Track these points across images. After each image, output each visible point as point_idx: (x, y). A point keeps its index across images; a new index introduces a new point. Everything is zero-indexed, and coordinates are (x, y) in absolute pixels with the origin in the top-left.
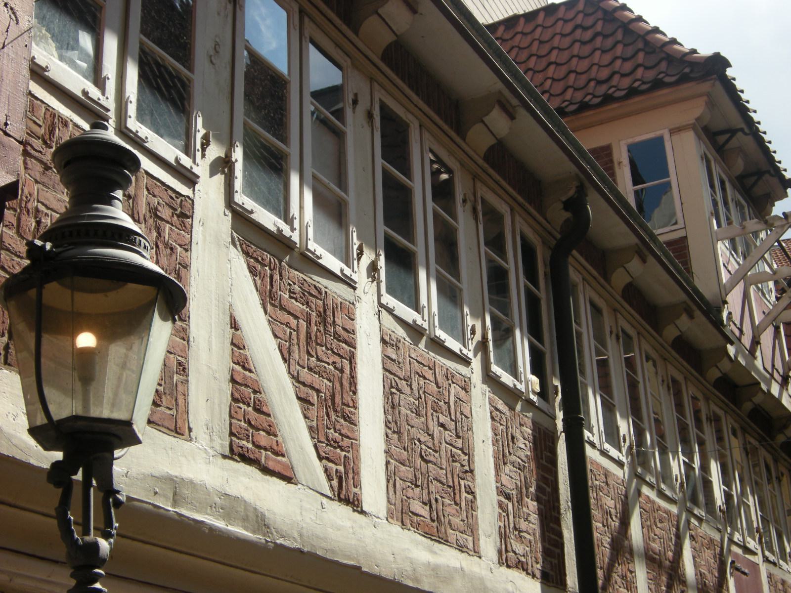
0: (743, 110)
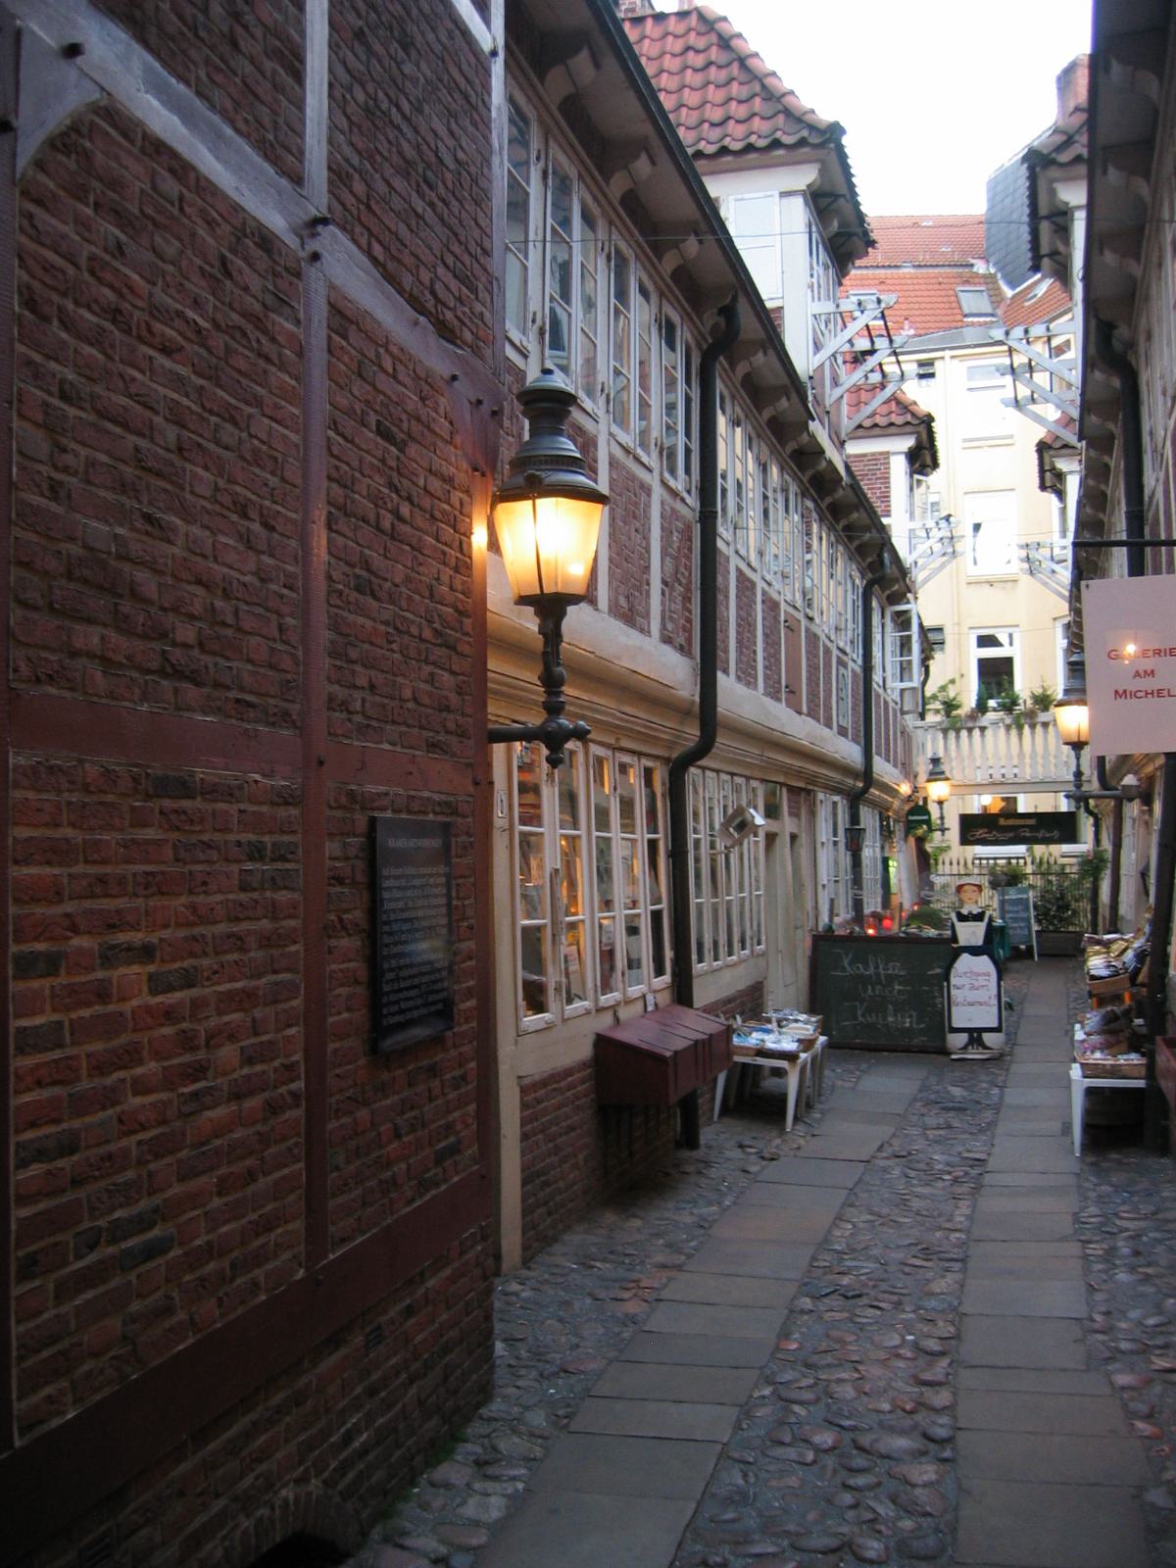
0: (851, 186)
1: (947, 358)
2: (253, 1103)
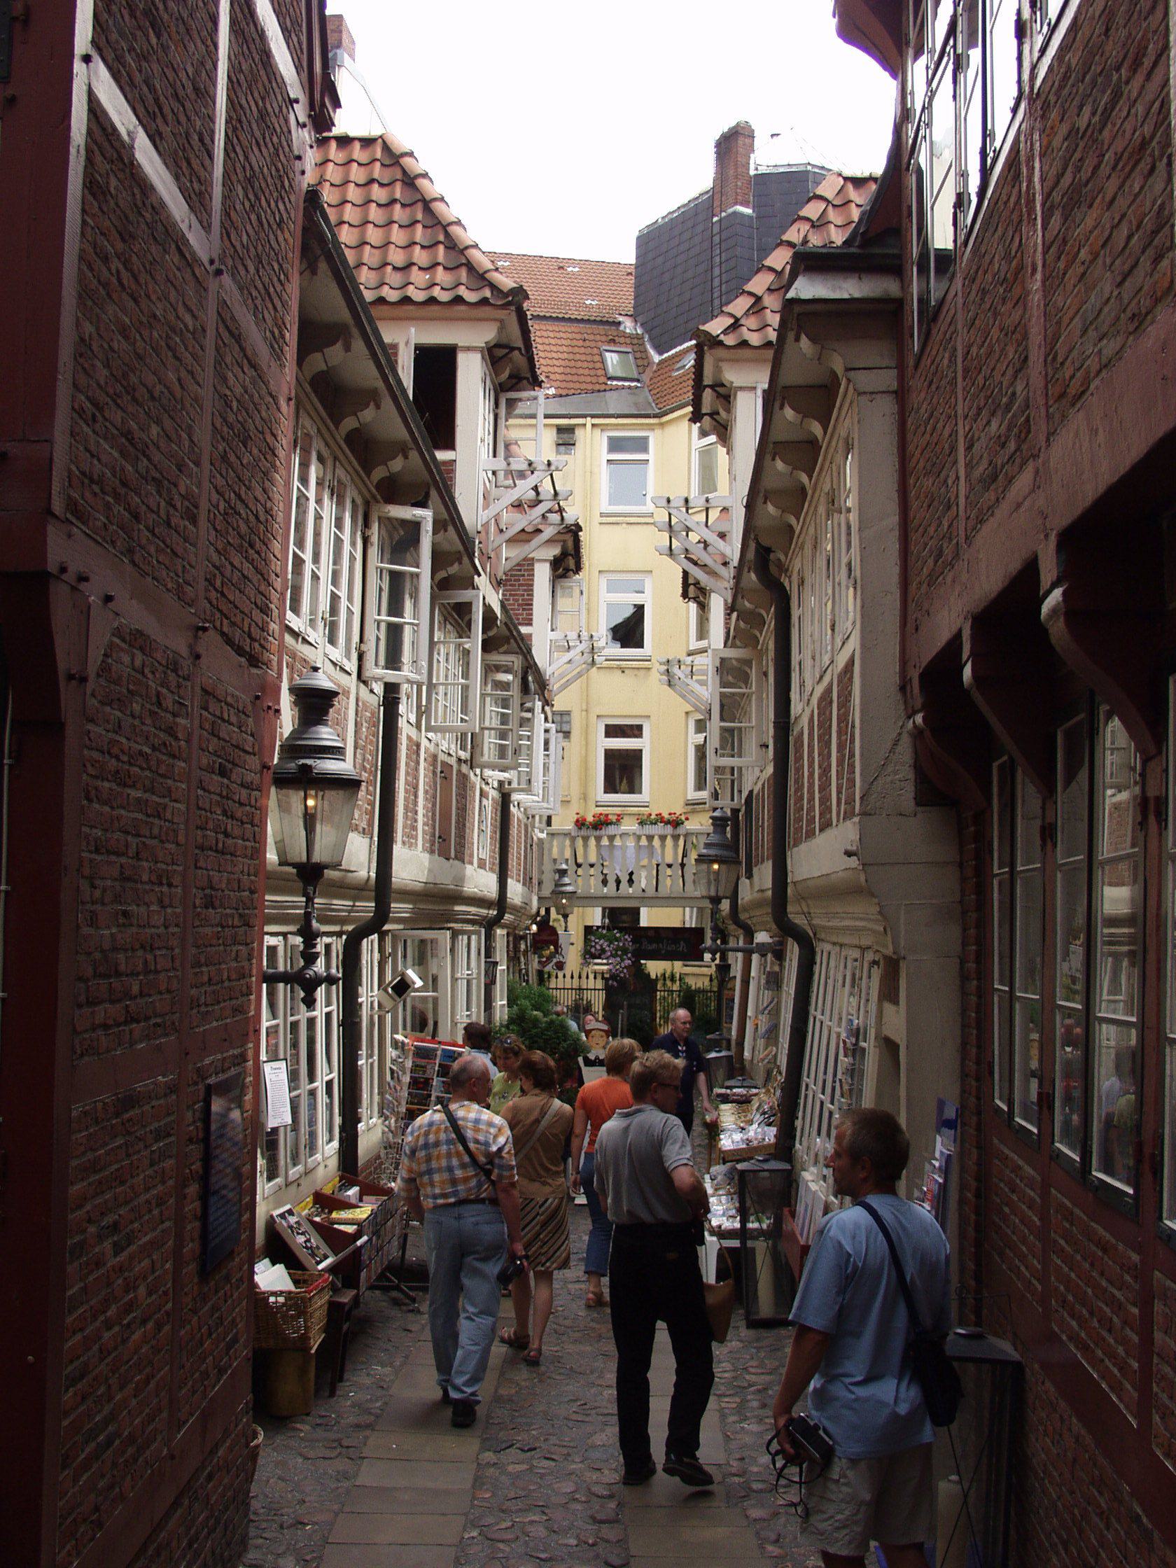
1: (589, 426)
2: (150, 1325)
